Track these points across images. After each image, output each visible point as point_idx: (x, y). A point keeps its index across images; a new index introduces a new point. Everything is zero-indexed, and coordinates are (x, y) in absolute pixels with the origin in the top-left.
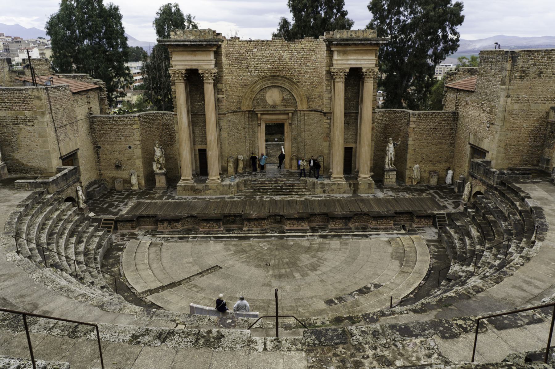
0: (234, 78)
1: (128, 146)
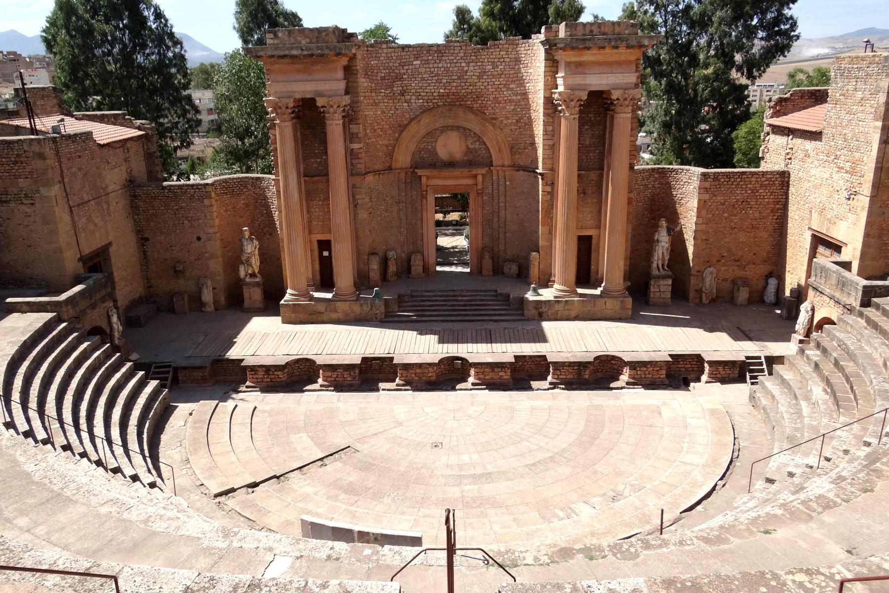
0: (379, 113)
1: (195, 236)
